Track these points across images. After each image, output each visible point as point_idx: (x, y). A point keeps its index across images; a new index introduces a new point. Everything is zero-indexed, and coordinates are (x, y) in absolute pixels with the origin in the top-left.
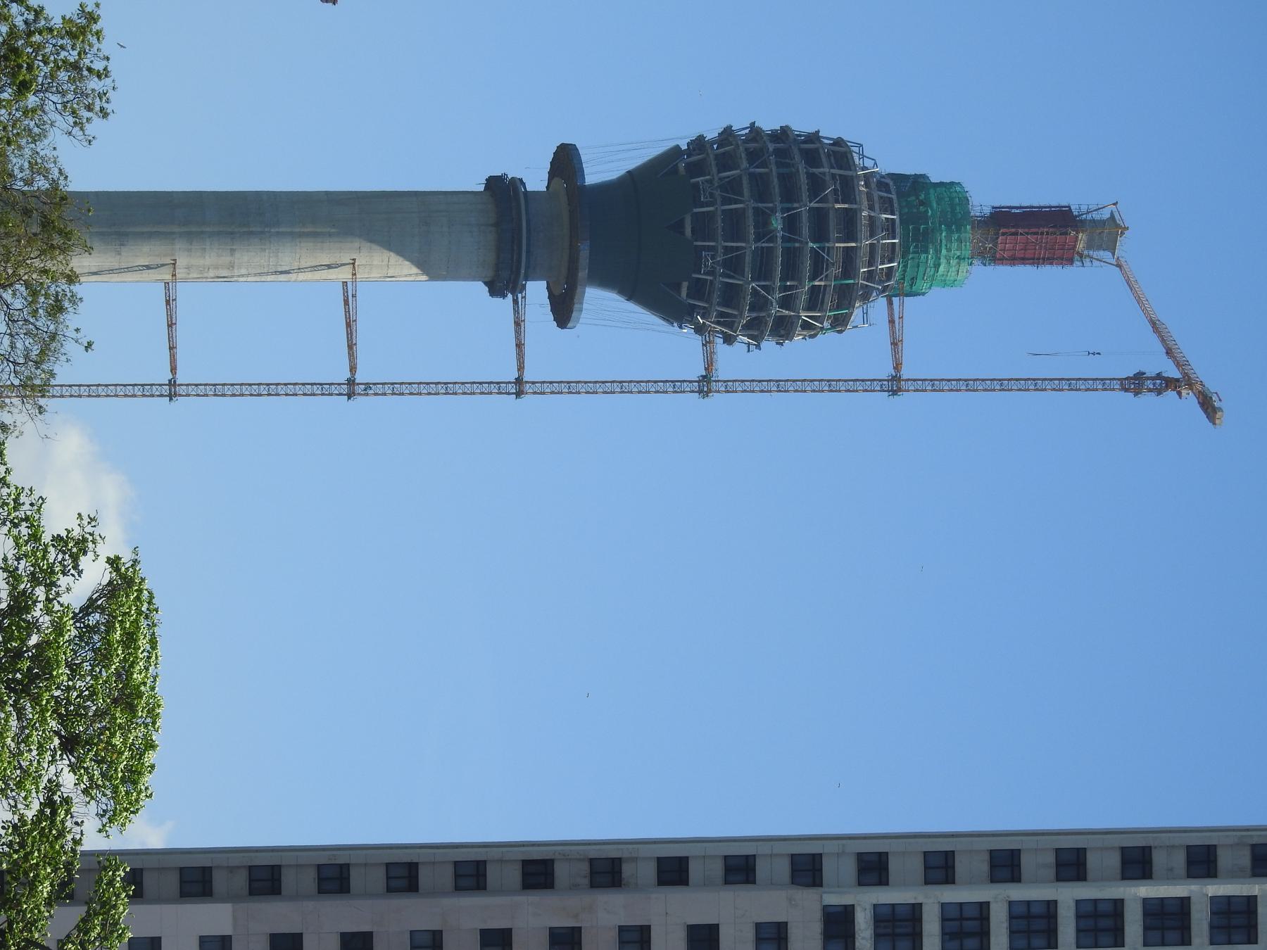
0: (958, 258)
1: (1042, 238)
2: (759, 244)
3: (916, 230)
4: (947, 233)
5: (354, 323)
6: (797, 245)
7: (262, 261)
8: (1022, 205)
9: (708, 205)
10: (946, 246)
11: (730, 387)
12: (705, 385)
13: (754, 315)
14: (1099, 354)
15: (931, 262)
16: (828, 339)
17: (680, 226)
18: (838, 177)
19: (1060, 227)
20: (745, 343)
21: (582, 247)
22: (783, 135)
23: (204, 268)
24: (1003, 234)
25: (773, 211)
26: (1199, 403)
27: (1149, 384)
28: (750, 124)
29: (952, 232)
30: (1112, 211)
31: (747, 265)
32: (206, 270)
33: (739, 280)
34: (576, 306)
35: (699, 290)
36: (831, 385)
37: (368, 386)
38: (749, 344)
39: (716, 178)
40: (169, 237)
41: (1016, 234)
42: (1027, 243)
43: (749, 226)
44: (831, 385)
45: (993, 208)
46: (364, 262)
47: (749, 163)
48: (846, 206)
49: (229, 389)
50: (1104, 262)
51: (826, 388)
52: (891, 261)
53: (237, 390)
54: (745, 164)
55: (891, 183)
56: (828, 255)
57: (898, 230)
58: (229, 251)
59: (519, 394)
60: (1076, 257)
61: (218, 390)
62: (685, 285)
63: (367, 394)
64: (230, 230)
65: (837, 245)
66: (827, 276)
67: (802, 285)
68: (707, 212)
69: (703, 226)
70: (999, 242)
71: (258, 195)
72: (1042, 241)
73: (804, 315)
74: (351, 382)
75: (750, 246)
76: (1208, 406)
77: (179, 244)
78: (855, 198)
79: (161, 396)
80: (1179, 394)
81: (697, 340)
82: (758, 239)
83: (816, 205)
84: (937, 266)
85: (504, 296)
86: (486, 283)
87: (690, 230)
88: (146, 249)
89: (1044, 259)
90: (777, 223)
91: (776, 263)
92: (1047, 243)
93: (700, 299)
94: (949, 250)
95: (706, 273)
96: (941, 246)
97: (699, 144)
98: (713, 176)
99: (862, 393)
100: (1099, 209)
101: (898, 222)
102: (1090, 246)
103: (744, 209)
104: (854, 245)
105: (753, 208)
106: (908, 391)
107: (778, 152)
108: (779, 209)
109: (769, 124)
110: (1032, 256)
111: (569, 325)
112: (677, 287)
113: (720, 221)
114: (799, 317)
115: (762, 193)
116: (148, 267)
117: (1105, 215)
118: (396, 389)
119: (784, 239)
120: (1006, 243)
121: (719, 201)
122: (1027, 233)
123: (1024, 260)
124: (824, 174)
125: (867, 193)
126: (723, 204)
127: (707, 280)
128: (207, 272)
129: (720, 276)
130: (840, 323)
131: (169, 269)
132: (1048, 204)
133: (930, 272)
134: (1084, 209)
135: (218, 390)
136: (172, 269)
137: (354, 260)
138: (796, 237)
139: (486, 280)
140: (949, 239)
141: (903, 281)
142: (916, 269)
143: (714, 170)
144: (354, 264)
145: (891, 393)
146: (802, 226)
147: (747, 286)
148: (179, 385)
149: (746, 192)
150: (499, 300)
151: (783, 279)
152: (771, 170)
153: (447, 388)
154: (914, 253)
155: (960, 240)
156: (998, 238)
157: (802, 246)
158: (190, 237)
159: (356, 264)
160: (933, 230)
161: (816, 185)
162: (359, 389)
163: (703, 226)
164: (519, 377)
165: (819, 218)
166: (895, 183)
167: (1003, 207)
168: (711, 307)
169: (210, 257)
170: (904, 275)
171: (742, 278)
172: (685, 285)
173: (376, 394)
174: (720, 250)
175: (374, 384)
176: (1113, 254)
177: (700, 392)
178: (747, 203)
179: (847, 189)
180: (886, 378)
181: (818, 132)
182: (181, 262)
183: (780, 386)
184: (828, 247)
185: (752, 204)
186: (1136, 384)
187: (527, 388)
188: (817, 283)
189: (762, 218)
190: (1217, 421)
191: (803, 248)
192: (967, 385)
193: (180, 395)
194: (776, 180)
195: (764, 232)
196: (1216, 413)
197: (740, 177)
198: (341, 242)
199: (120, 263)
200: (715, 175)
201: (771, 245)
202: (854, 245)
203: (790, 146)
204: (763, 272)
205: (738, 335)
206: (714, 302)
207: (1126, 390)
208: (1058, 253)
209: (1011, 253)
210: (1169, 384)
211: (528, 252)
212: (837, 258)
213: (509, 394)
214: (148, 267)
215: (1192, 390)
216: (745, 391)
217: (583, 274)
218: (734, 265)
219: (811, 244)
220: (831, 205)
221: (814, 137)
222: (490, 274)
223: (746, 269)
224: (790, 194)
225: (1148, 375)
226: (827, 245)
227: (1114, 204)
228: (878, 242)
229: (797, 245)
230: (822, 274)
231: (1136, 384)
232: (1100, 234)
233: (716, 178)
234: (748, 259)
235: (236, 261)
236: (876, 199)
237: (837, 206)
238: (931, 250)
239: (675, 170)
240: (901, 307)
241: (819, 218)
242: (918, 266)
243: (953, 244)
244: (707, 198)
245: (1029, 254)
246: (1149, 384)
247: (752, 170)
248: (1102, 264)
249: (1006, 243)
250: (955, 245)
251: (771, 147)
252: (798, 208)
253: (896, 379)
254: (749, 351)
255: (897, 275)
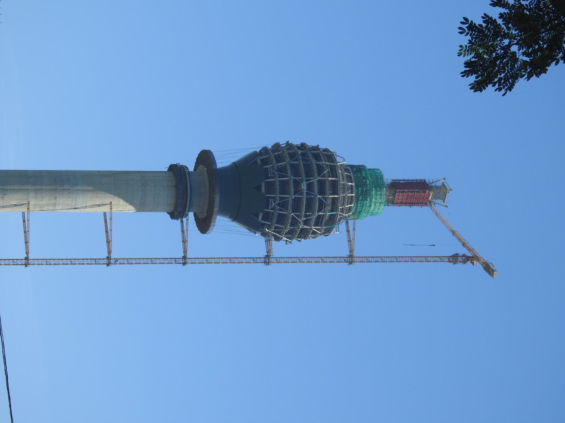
0: (380, 203)
1: (414, 194)
2: (295, 196)
3: (362, 190)
4: (375, 192)
5: (28, 232)
6: (312, 196)
7: (69, 203)
8: (405, 179)
9: (270, 178)
10: (375, 197)
11: (278, 260)
12: (267, 259)
13: (292, 228)
14: (434, 245)
15: (368, 204)
16: (321, 238)
17: (258, 188)
18: (329, 166)
19: (423, 189)
20: (285, 241)
21: (216, 197)
22: (303, 146)
23: (42, 206)
24: (398, 192)
25: (302, 181)
26: (483, 267)
27: (460, 259)
28: (287, 142)
29: (377, 191)
30: (443, 182)
31: (289, 205)
32: (43, 207)
33: (285, 212)
34: (212, 224)
35: (267, 217)
36: (323, 260)
37: (116, 260)
38: (287, 241)
39: (276, 166)
40: (27, 191)
41: (403, 192)
42: (408, 196)
43: (291, 187)
44: (323, 260)
45: (392, 180)
46: (115, 203)
47: (290, 159)
48: (334, 179)
49: (3, 262)
50: (440, 205)
51: (174, 262)
52: (351, 204)
53: (56, 262)
54: (288, 160)
55: (350, 169)
56: (325, 200)
57: (354, 190)
58: (54, 198)
59: (184, 264)
60: (428, 203)
61: (47, 262)
62: (261, 214)
63: (116, 264)
64: (54, 188)
65: (330, 196)
66: (324, 211)
67: (314, 214)
68: (270, 181)
69: (270, 187)
70: (396, 196)
71: (75, 172)
72: (414, 195)
73: (314, 228)
74: (108, 258)
75: (291, 197)
76: (488, 269)
77: (31, 195)
78: (337, 175)
79: (22, 264)
80: (473, 263)
81: (262, 240)
82: (295, 194)
83: (320, 178)
84: (370, 206)
85: (177, 219)
86: (168, 213)
87: (264, 189)
88: (16, 196)
89: (414, 203)
90: (304, 187)
91: (303, 205)
92: (417, 196)
93: (267, 221)
94: (376, 199)
95: (271, 209)
96: (372, 198)
97: (265, 150)
98: (274, 164)
99: (142, 265)
100: (437, 181)
101: (354, 186)
102: (435, 197)
103: (288, 180)
104: (337, 196)
105: (293, 179)
106: (357, 262)
107: (302, 154)
108: (304, 180)
109: (296, 142)
110: (410, 202)
111: (207, 232)
112: (257, 215)
113: (278, 186)
114: (311, 229)
115: (296, 173)
116: (16, 205)
117: (439, 184)
118: (129, 261)
119: (307, 194)
120: (399, 196)
121: (277, 176)
122: (409, 192)
123: (406, 204)
124: (323, 164)
125: (342, 173)
126: (279, 177)
127: (271, 212)
128: (44, 207)
129: (278, 210)
130: (327, 232)
131: (26, 206)
132: (415, 179)
133: (367, 209)
134: (431, 181)
135: (47, 262)
136: (27, 206)
137: (111, 202)
138: (312, 193)
139: (169, 212)
140: (376, 194)
141: (355, 213)
142: (362, 207)
143: (274, 162)
144: (111, 204)
145: (349, 263)
146: (314, 188)
147: (289, 215)
148: (30, 260)
149: (289, 172)
150: (175, 221)
151: (305, 212)
152: (300, 162)
153: (72, 262)
154: (361, 200)
155: (381, 195)
156: (395, 194)
157: (315, 197)
158: (36, 191)
159: (112, 204)
160: (369, 190)
161: (320, 169)
162: (113, 261)
163: (270, 187)
164: (184, 256)
165: (321, 184)
166: (351, 169)
167: (396, 180)
168: (272, 224)
169: (45, 200)
170: (356, 210)
171: (287, 211)
172: (261, 214)
173: (120, 264)
174: (278, 199)
175: (119, 259)
176: (444, 201)
177: (265, 262)
178: (290, 177)
179: (333, 171)
180: (346, 256)
181: (318, 146)
182: (32, 202)
183: (300, 260)
184: (326, 197)
185: (293, 178)
186: (454, 259)
187: (189, 261)
188: (320, 214)
189: (297, 184)
190: (494, 276)
191: (315, 198)
192: (175, 261)
193: (31, 264)
194: (302, 167)
195: (297, 190)
196: (494, 272)
197: (286, 166)
198: (106, 194)
199: (3, 203)
200: (275, 165)
201: (301, 196)
202: (337, 196)
203: (307, 152)
204: (296, 208)
205: (283, 237)
206: (274, 222)
207: (450, 262)
208: (421, 201)
209: (401, 201)
210: (467, 259)
211: (190, 198)
212: (329, 202)
213: (180, 263)
214: (16, 205)
215: (478, 261)
216: (136, 263)
217: (216, 209)
218: (283, 205)
219: (318, 196)
220: (327, 178)
221: (317, 148)
222: (171, 209)
223: (289, 207)
224: (309, 174)
225: (460, 255)
226: (325, 196)
227: (444, 179)
228: (346, 195)
229: (312, 196)
230: (322, 210)
231: (454, 259)
232: (439, 192)
233: (276, 166)
234: (290, 203)
235: (57, 202)
236: (344, 176)
237: (330, 179)
238: (369, 199)
239: (256, 163)
240: (354, 224)
241: (321, 184)
242: (363, 206)
243: (378, 197)
244: (271, 175)
245: (409, 201)
246: (460, 259)
247: (291, 162)
248: (440, 205)
249: (399, 196)
250: (378, 197)
251: (300, 152)
252: (313, 180)
253: (351, 256)
254: (286, 244)
255: (353, 210)
